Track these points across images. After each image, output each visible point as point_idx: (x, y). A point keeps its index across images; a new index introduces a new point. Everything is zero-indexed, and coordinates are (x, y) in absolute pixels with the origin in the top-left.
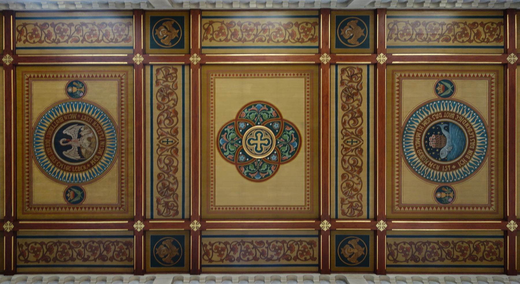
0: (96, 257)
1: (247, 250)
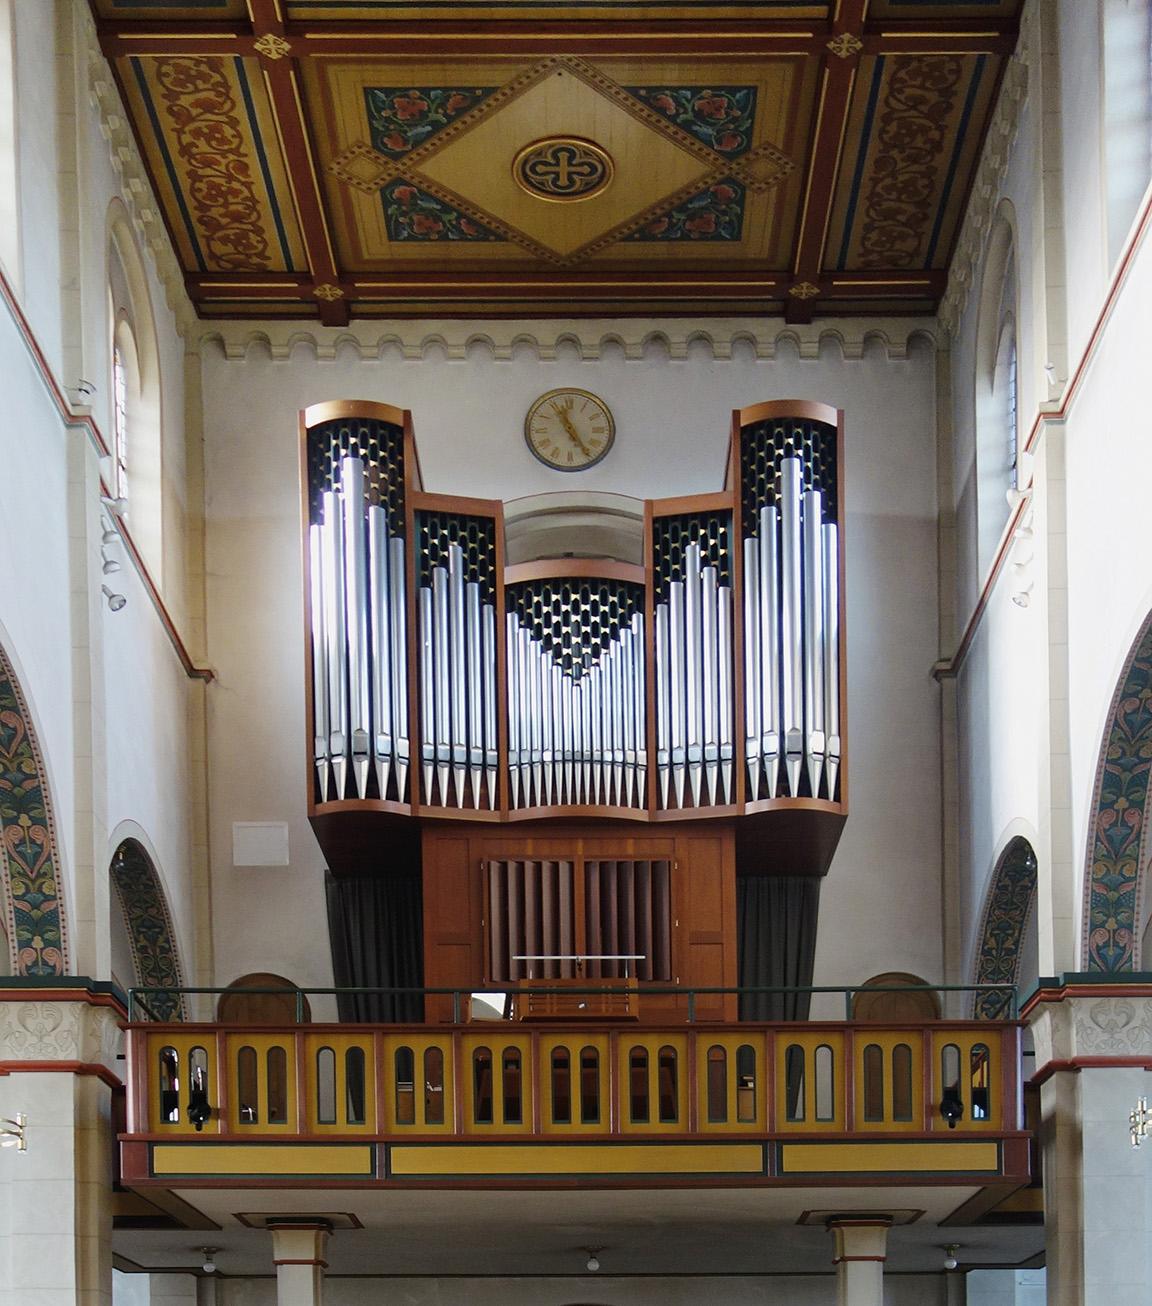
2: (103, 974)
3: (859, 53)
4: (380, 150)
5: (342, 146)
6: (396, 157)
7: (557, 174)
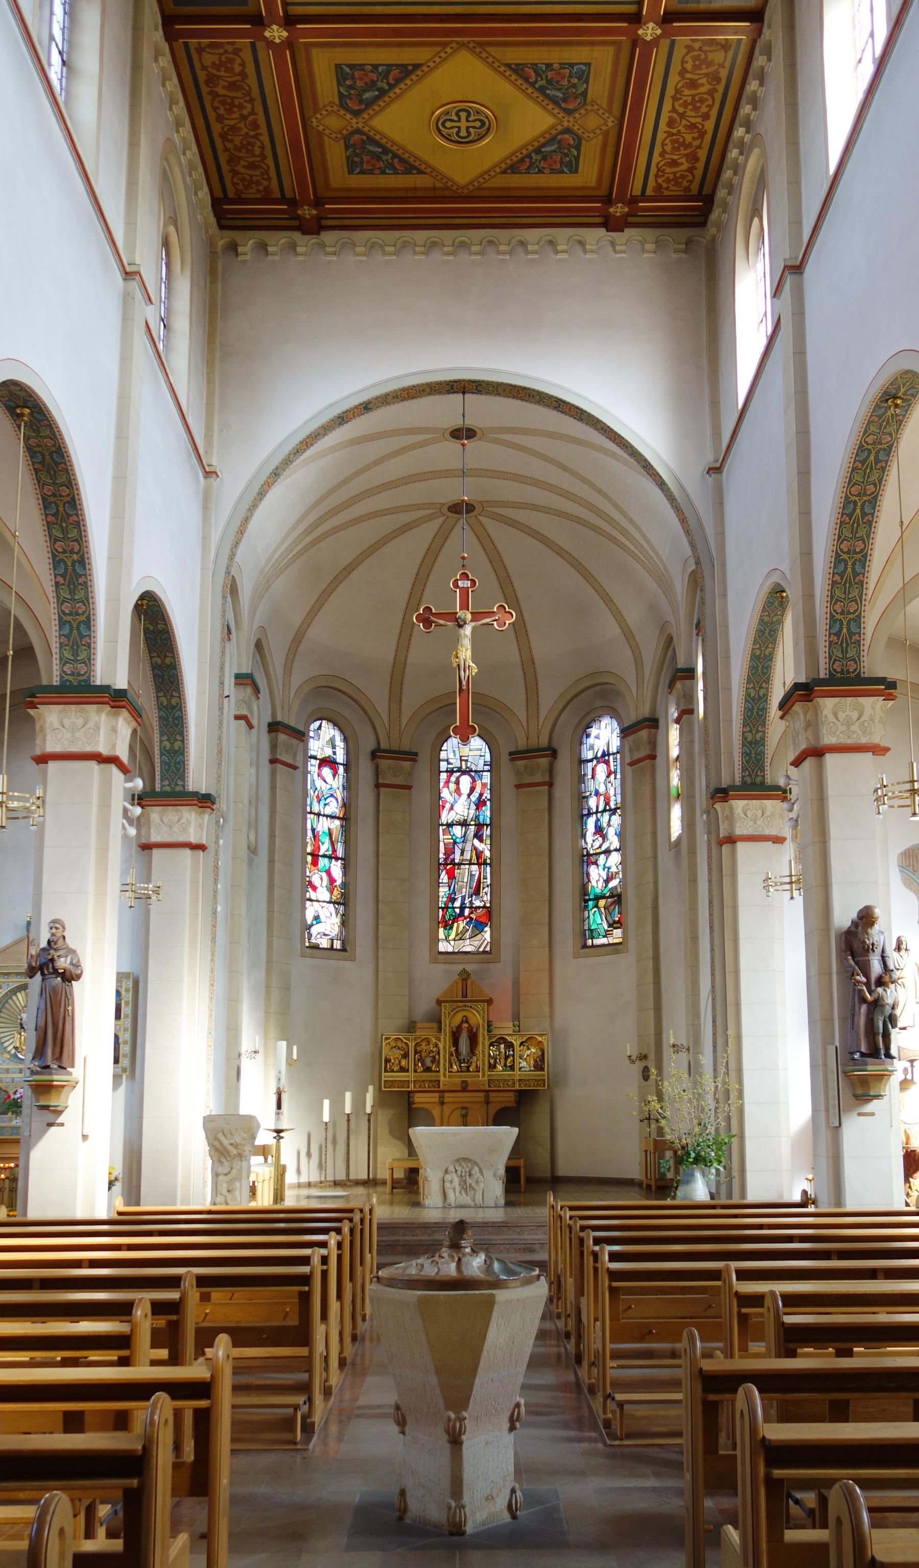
0: (210, 69)
1: (236, 106)
2: (121, 682)
3: (659, 37)
4: (576, 135)
5: (321, 105)
6: (567, 131)
7: (459, 128)
